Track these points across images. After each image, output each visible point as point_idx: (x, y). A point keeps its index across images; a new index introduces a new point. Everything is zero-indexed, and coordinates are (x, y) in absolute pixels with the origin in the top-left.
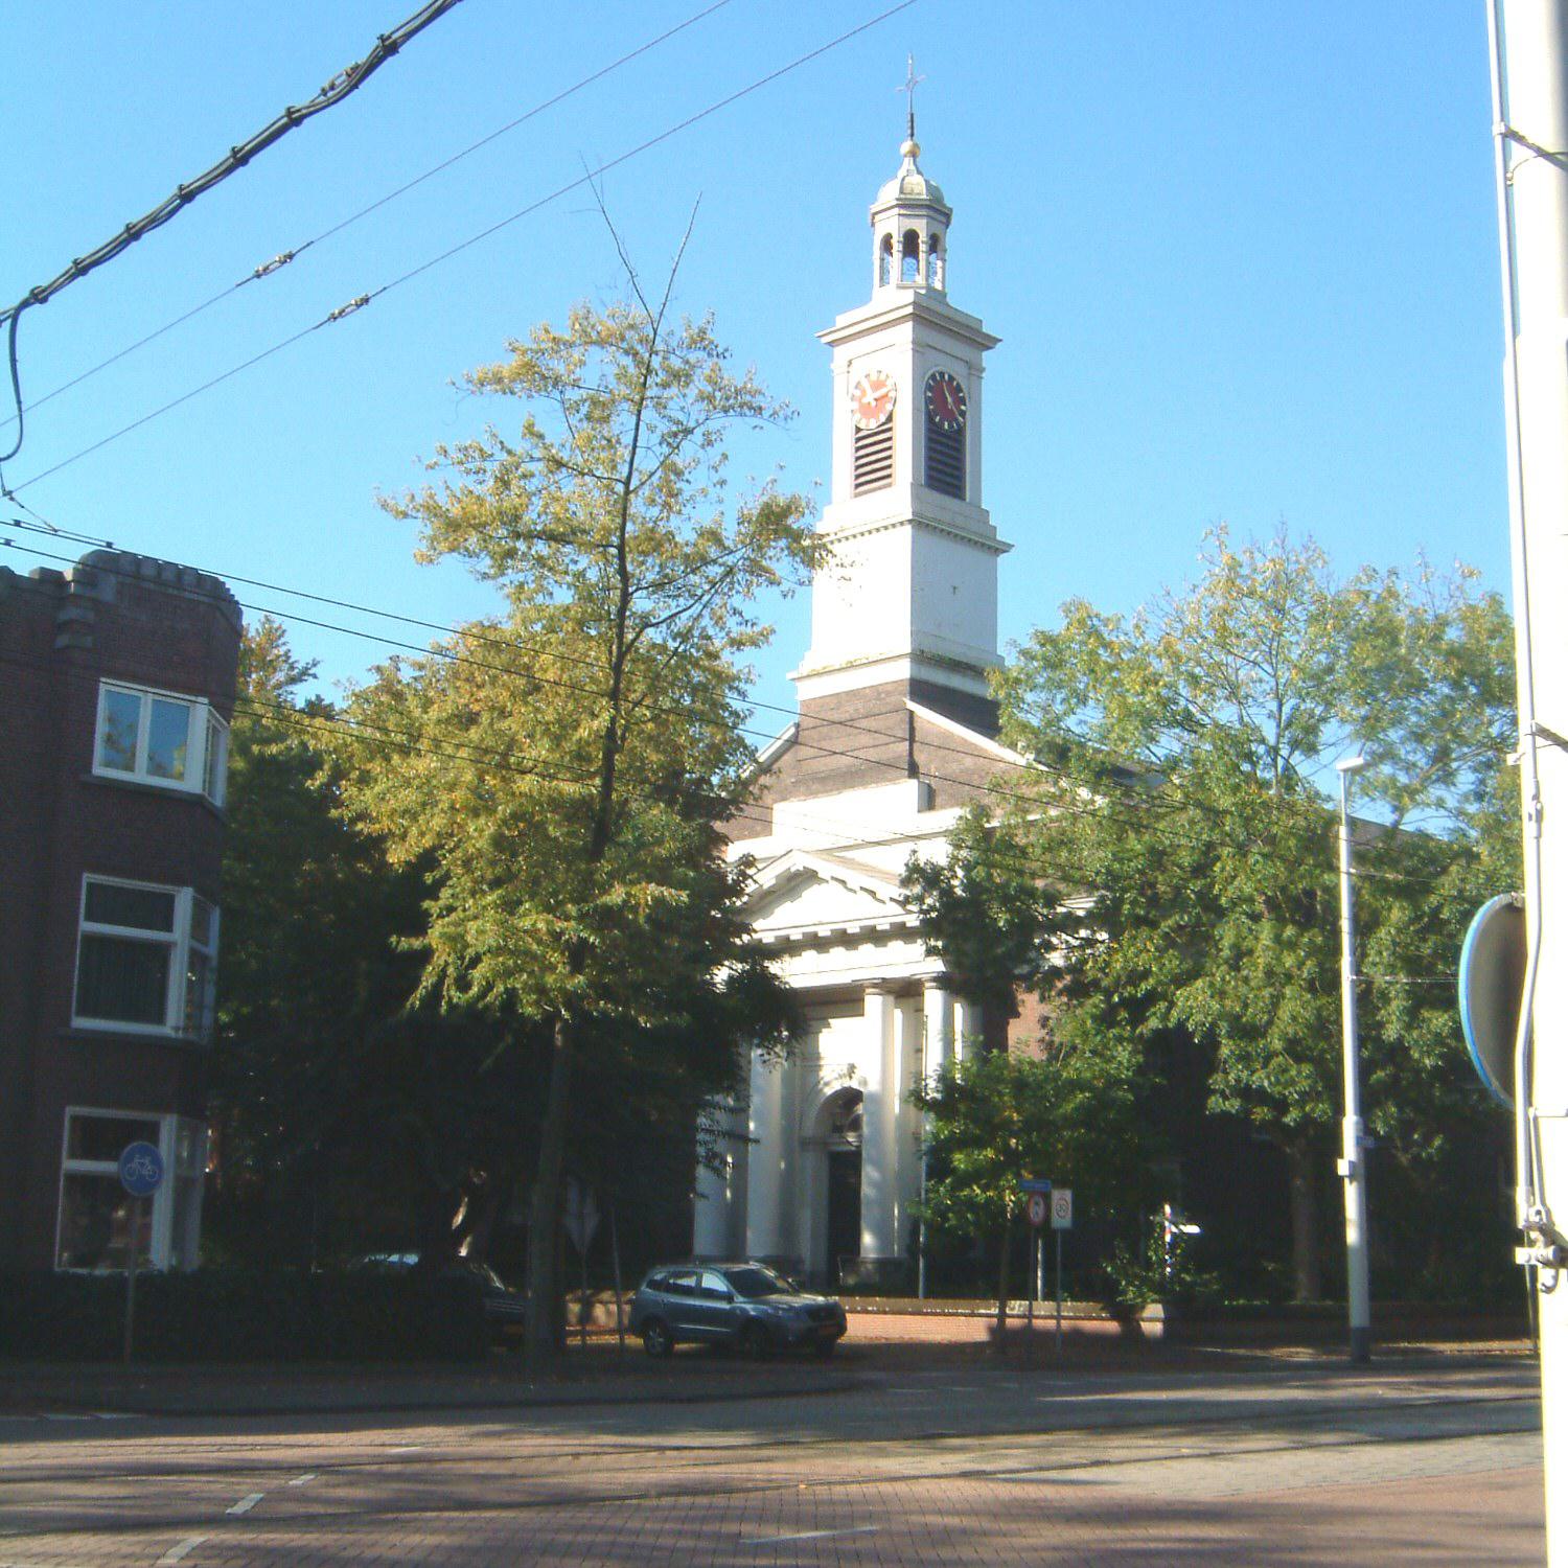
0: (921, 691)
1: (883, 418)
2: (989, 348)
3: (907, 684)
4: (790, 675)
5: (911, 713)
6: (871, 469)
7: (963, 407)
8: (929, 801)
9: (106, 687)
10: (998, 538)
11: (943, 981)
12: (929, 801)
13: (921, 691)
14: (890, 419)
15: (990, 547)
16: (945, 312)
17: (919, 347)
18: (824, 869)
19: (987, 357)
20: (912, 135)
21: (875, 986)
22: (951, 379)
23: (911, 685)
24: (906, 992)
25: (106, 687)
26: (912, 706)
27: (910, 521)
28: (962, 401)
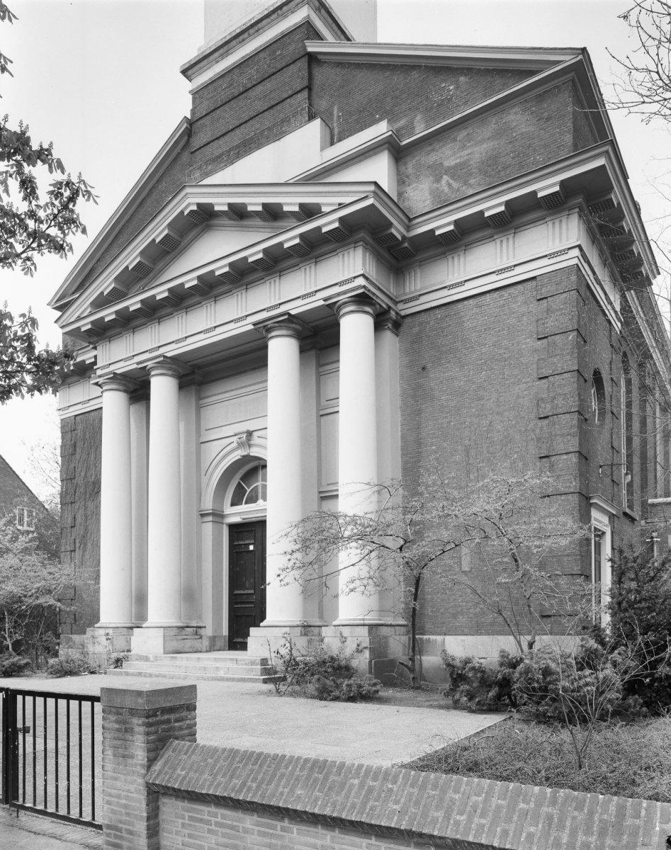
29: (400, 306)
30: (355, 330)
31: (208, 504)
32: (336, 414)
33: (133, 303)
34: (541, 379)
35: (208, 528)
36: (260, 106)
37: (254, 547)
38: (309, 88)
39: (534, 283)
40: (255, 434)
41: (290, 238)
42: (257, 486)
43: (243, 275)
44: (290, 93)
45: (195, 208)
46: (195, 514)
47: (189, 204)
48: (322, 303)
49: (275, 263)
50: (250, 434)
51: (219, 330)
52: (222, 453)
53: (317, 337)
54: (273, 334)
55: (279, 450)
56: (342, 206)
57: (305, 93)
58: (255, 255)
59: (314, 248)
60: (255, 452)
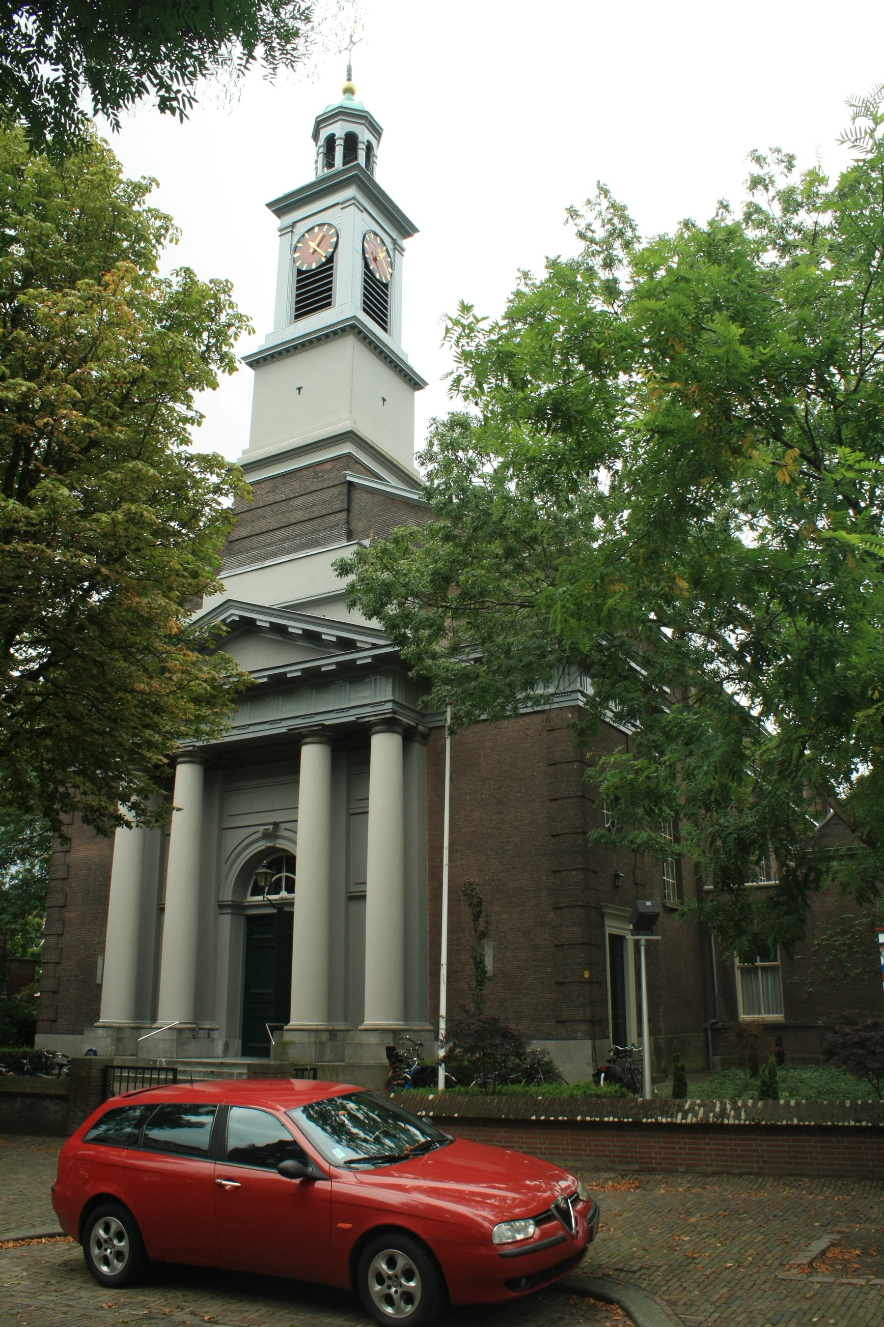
29: (430, 719)
30: (384, 749)
31: (227, 896)
32: (362, 816)
34: (552, 800)
35: (226, 921)
36: (300, 515)
37: (590, 974)
38: (348, 510)
39: (544, 716)
40: (283, 826)
41: (328, 663)
42: (281, 878)
43: (279, 687)
44: (330, 511)
45: (237, 619)
46: (213, 906)
47: (232, 615)
48: (353, 718)
49: (314, 681)
50: (276, 825)
51: (251, 729)
52: (245, 841)
53: (349, 749)
54: (307, 740)
55: (308, 840)
56: (375, 646)
57: (345, 513)
58: (294, 673)
59: (351, 675)
60: (281, 844)
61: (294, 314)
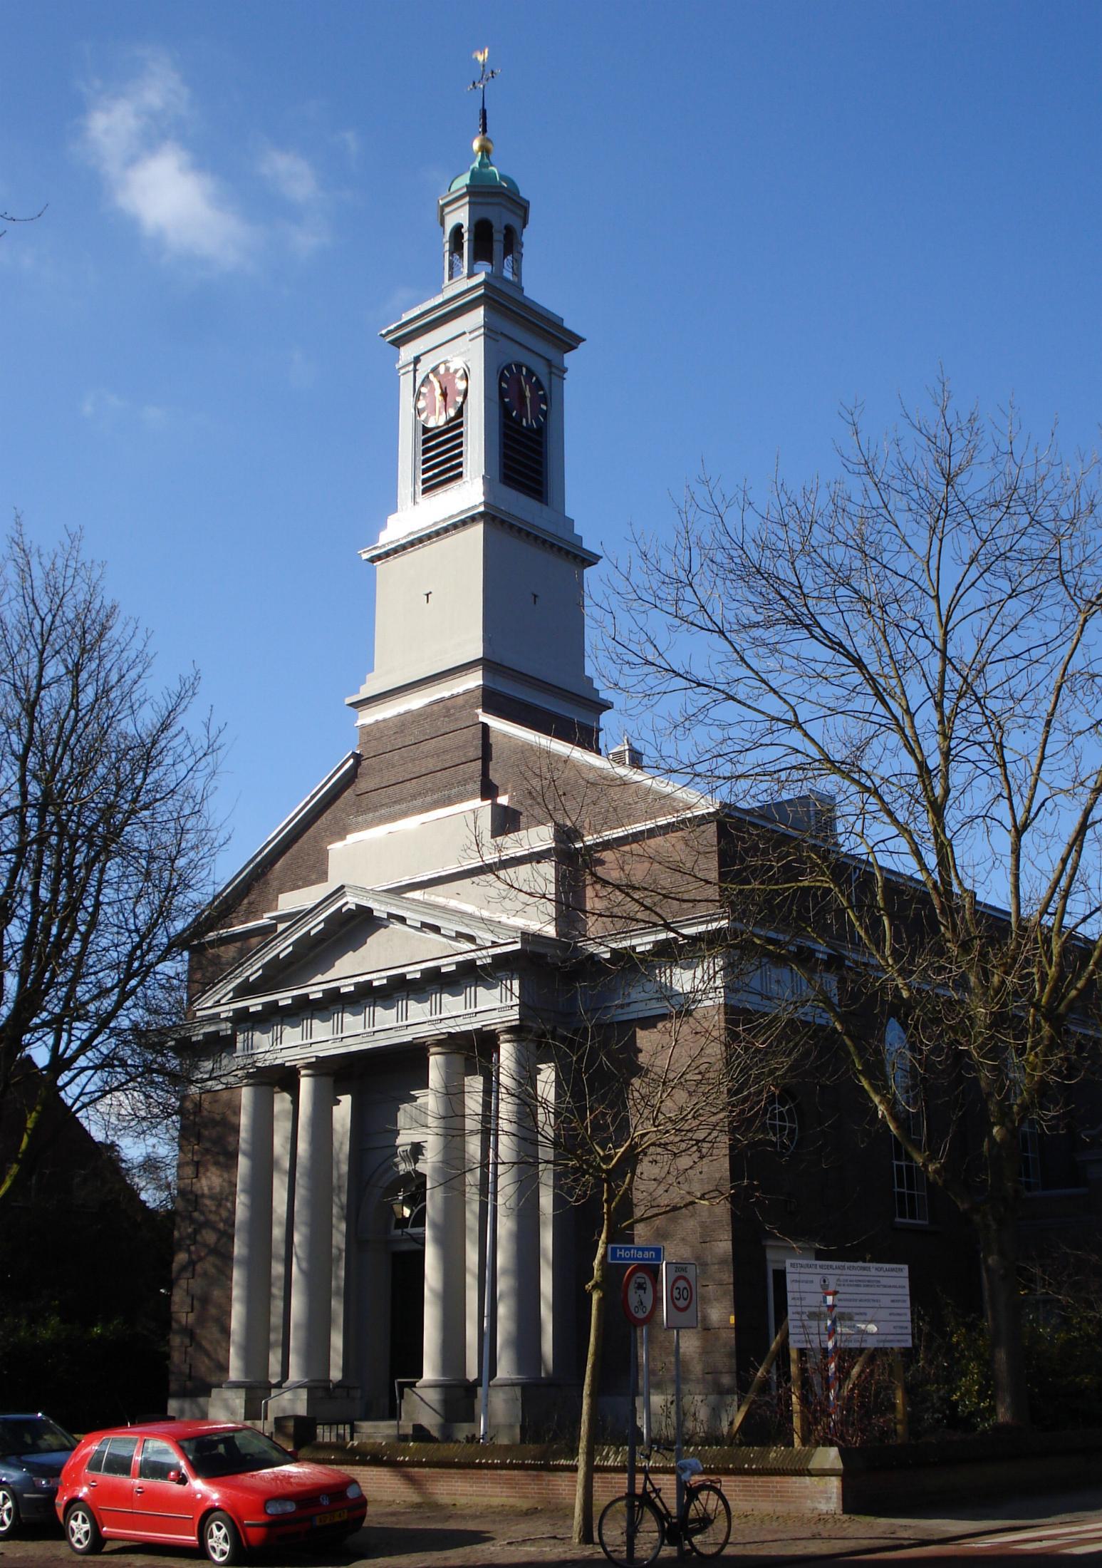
0: (493, 701)
1: (452, 413)
2: (573, 348)
3: (480, 692)
4: (349, 700)
5: (485, 727)
6: (440, 463)
7: (544, 407)
8: (506, 822)
9: (906, 1267)
10: (585, 546)
11: (516, 1032)
12: (506, 822)
13: (493, 701)
14: (460, 413)
15: (576, 556)
16: (520, 299)
17: (491, 333)
18: (380, 910)
19: (570, 359)
20: (485, 131)
21: (439, 1043)
22: (531, 373)
23: (483, 696)
24: (473, 1050)
25: (906, 1267)
26: (484, 718)
27: (482, 515)
28: (544, 399)
33: (284, 998)
36: (431, 764)
61: (420, 487)
